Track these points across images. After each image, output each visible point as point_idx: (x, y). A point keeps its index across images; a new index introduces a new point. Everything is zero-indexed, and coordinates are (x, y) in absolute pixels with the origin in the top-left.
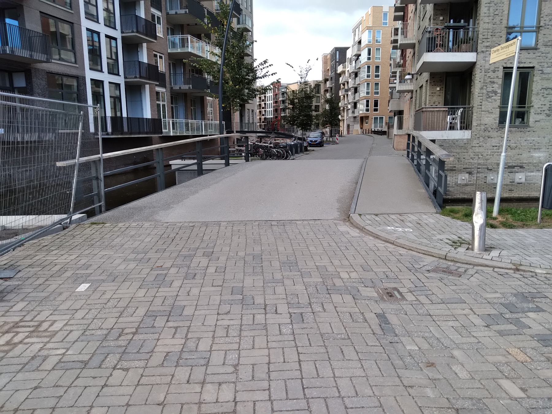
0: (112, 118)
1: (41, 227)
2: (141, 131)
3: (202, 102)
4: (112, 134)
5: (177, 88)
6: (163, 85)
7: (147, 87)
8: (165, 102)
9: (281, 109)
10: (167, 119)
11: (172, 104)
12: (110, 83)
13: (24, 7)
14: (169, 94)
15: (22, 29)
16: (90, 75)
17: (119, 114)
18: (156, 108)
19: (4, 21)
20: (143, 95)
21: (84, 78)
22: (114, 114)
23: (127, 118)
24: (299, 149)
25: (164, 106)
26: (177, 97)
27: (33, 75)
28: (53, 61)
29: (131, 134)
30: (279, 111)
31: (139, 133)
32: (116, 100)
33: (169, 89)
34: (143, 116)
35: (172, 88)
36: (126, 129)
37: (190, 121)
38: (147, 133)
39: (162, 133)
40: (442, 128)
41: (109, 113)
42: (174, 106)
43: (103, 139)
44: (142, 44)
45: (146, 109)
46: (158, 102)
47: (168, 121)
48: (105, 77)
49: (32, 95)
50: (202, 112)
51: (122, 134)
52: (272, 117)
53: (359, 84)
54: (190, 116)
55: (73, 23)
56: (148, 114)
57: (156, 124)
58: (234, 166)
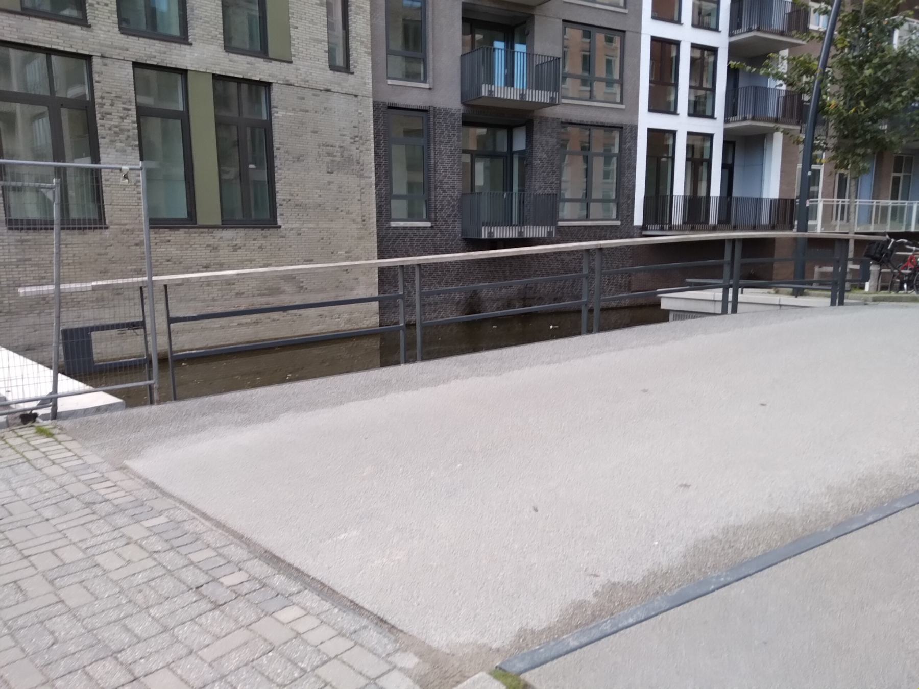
1: (478, 375)
7: (778, 138)
13: (536, 17)
15: (530, 55)
16: (648, 121)
17: (702, 193)
19: (492, 45)
21: (634, 129)
24: (730, 306)
27: (535, 129)
28: (564, 101)
34: (761, 192)
40: (410, 345)
42: (901, 175)
43: (798, 231)
48: (682, 124)
49: (64, 161)
55: (624, 31)
58: (679, 324)
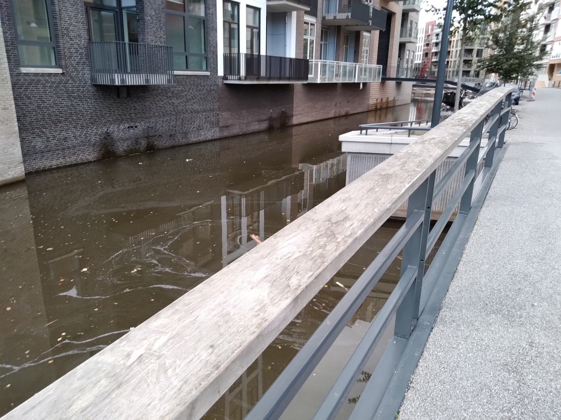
0: (246, 55)
2: (282, 75)
3: (357, 37)
4: (246, 79)
5: (330, 17)
6: (313, 13)
7: (294, 14)
8: (313, 36)
9: (433, 53)
10: (314, 60)
11: (322, 40)
12: (248, 6)
14: (320, 26)
18: (303, 45)
20: (288, 26)
22: (249, 50)
23: (266, 56)
25: (312, 42)
26: (330, 30)
29: (270, 79)
30: (430, 56)
31: (280, 79)
32: (254, 31)
33: (320, 19)
35: (324, 18)
36: (263, 73)
37: (342, 63)
38: (289, 79)
39: (307, 79)
41: (243, 50)
42: (323, 43)
44: (291, 12)
45: (290, 45)
46: (305, 37)
47: (316, 63)
50: (355, 52)
51: (258, 78)
52: (420, 62)
53: (557, 19)
54: (341, 57)
56: (291, 52)
57: (301, 67)
